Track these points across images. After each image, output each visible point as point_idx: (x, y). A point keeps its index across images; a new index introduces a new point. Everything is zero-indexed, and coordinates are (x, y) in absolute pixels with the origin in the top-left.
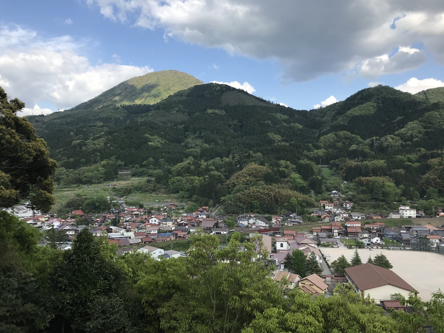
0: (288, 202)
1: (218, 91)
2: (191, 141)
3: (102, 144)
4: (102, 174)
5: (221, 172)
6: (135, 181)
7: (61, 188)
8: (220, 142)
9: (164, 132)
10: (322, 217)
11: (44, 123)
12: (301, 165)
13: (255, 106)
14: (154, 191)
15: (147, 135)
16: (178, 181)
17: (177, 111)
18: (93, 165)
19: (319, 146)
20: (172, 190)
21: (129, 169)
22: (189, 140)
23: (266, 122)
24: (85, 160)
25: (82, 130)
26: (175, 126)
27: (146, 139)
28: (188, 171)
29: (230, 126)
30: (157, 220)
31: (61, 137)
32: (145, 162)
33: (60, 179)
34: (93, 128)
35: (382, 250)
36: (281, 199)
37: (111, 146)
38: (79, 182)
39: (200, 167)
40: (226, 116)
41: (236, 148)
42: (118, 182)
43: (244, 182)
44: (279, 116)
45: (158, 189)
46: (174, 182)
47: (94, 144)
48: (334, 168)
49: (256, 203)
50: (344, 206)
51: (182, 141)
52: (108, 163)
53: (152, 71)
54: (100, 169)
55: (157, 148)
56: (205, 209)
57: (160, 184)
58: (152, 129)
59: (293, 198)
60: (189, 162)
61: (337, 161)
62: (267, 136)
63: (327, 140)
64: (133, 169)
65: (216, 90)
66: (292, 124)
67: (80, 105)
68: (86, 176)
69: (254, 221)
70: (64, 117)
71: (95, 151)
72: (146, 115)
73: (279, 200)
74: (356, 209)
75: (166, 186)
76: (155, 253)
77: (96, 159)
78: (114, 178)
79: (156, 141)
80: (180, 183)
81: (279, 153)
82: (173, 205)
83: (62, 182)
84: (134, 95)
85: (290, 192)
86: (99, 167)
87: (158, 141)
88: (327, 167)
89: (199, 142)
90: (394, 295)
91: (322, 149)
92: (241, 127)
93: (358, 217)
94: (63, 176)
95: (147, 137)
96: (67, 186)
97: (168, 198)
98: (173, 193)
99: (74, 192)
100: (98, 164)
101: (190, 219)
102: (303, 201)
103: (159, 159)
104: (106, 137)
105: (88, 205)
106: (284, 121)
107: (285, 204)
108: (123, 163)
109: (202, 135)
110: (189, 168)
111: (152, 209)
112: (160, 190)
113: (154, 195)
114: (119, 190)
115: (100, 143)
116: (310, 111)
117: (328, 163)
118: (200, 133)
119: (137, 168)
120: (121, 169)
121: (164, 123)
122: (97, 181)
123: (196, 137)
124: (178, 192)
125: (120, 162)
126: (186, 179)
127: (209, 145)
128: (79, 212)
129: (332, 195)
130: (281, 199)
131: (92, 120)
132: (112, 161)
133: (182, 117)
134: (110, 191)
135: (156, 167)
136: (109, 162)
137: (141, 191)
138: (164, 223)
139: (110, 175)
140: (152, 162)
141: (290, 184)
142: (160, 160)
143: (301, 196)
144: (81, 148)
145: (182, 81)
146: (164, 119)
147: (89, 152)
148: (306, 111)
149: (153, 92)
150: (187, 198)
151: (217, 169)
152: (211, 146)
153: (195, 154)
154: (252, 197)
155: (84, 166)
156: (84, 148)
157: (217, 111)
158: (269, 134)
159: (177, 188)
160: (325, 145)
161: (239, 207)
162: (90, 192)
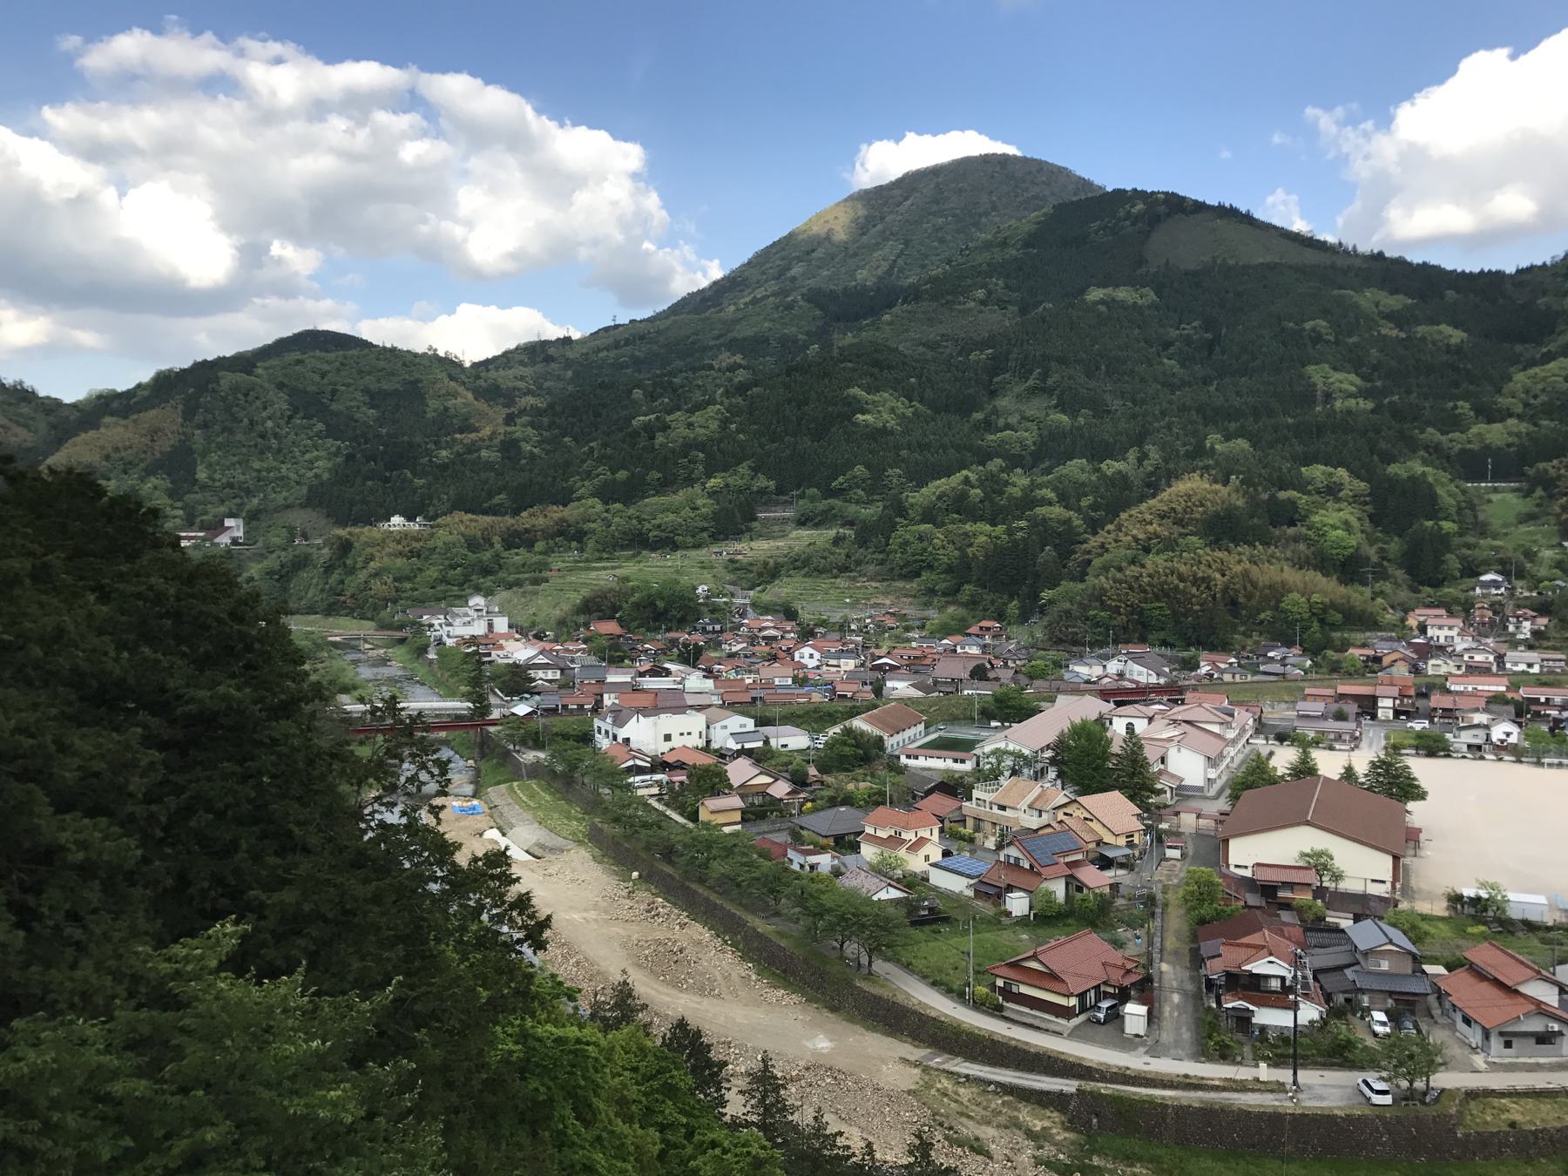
0: (1276, 608)
1: (1136, 219)
3: (714, 425)
4: (705, 518)
5: (1079, 510)
6: (801, 539)
7: (587, 561)
8: (1116, 404)
9: (919, 377)
10: (1386, 661)
11: (569, 364)
12: (1393, 482)
13: (1272, 267)
14: (844, 569)
15: (856, 391)
16: (921, 539)
18: (681, 493)
19: (1499, 411)
22: (1003, 403)
23: (1308, 325)
25: (670, 383)
26: (960, 354)
27: (850, 404)
28: (959, 505)
29: (1167, 345)
30: (817, 655)
31: (604, 406)
32: (841, 479)
35: (1517, 765)
36: (1249, 597)
37: (738, 431)
38: (640, 542)
39: (1001, 493)
40: (1157, 308)
41: (1169, 427)
42: (753, 544)
43: (1136, 540)
44: (1370, 299)
45: (858, 563)
46: (906, 543)
47: (690, 425)
48: (1539, 492)
49: (1158, 609)
50: (1511, 628)
51: (975, 406)
52: (727, 485)
53: (1019, 154)
54: (699, 502)
55: (884, 432)
56: (988, 629)
58: (876, 370)
59: (1295, 596)
61: (1550, 467)
62: (1301, 376)
63: (1540, 386)
64: (801, 502)
66: (1421, 330)
67: (684, 299)
69: (1120, 666)
70: (627, 342)
71: (689, 446)
72: (873, 323)
73: (1241, 600)
74: (1548, 639)
78: (742, 532)
79: (883, 410)
80: (925, 544)
81: (1323, 437)
82: (893, 614)
83: (591, 544)
85: (1291, 575)
87: (892, 410)
88: (1514, 490)
90: (1308, 855)
91: (1511, 422)
92: (1210, 347)
93: (1530, 665)
94: (593, 525)
95: (855, 397)
96: (605, 555)
97: (886, 593)
98: (903, 577)
99: (618, 572)
100: (697, 487)
101: (918, 653)
102: (1333, 605)
104: (726, 402)
105: (637, 606)
106: (1390, 317)
107: (1262, 616)
108: (772, 484)
109: (1050, 381)
110: (963, 496)
113: (842, 582)
114: (747, 568)
115: (706, 423)
116: (1520, 272)
117: (1519, 475)
118: (1044, 376)
119: (813, 499)
120: (766, 504)
121: (932, 346)
122: (689, 540)
123: (1027, 390)
124: (919, 575)
125: (762, 482)
127: (1074, 415)
128: (611, 627)
129: (1478, 591)
130: (1249, 597)
131: (711, 348)
132: (740, 476)
133: (996, 320)
134: (720, 571)
136: (730, 480)
138: (832, 662)
139: (731, 522)
140: (864, 481)
141: (1302, 547)
143: (1327, 588)
144: (652, 438)
145: (1027, 189)
146: (932, 334)
147: (673, 451)
148: (1499, 275)
150: (945, 594)
151: (1063, 499)
152: (1081, 420)
153: (1017, 449)
154: (1145, 591)
155: (657, 493)
156: (660, 439)
157: (1123, 294)
158: (1311, 369)
159: (916, 561)
160: (1526, 405)
161: (1097, 625)
162: (652, 570)
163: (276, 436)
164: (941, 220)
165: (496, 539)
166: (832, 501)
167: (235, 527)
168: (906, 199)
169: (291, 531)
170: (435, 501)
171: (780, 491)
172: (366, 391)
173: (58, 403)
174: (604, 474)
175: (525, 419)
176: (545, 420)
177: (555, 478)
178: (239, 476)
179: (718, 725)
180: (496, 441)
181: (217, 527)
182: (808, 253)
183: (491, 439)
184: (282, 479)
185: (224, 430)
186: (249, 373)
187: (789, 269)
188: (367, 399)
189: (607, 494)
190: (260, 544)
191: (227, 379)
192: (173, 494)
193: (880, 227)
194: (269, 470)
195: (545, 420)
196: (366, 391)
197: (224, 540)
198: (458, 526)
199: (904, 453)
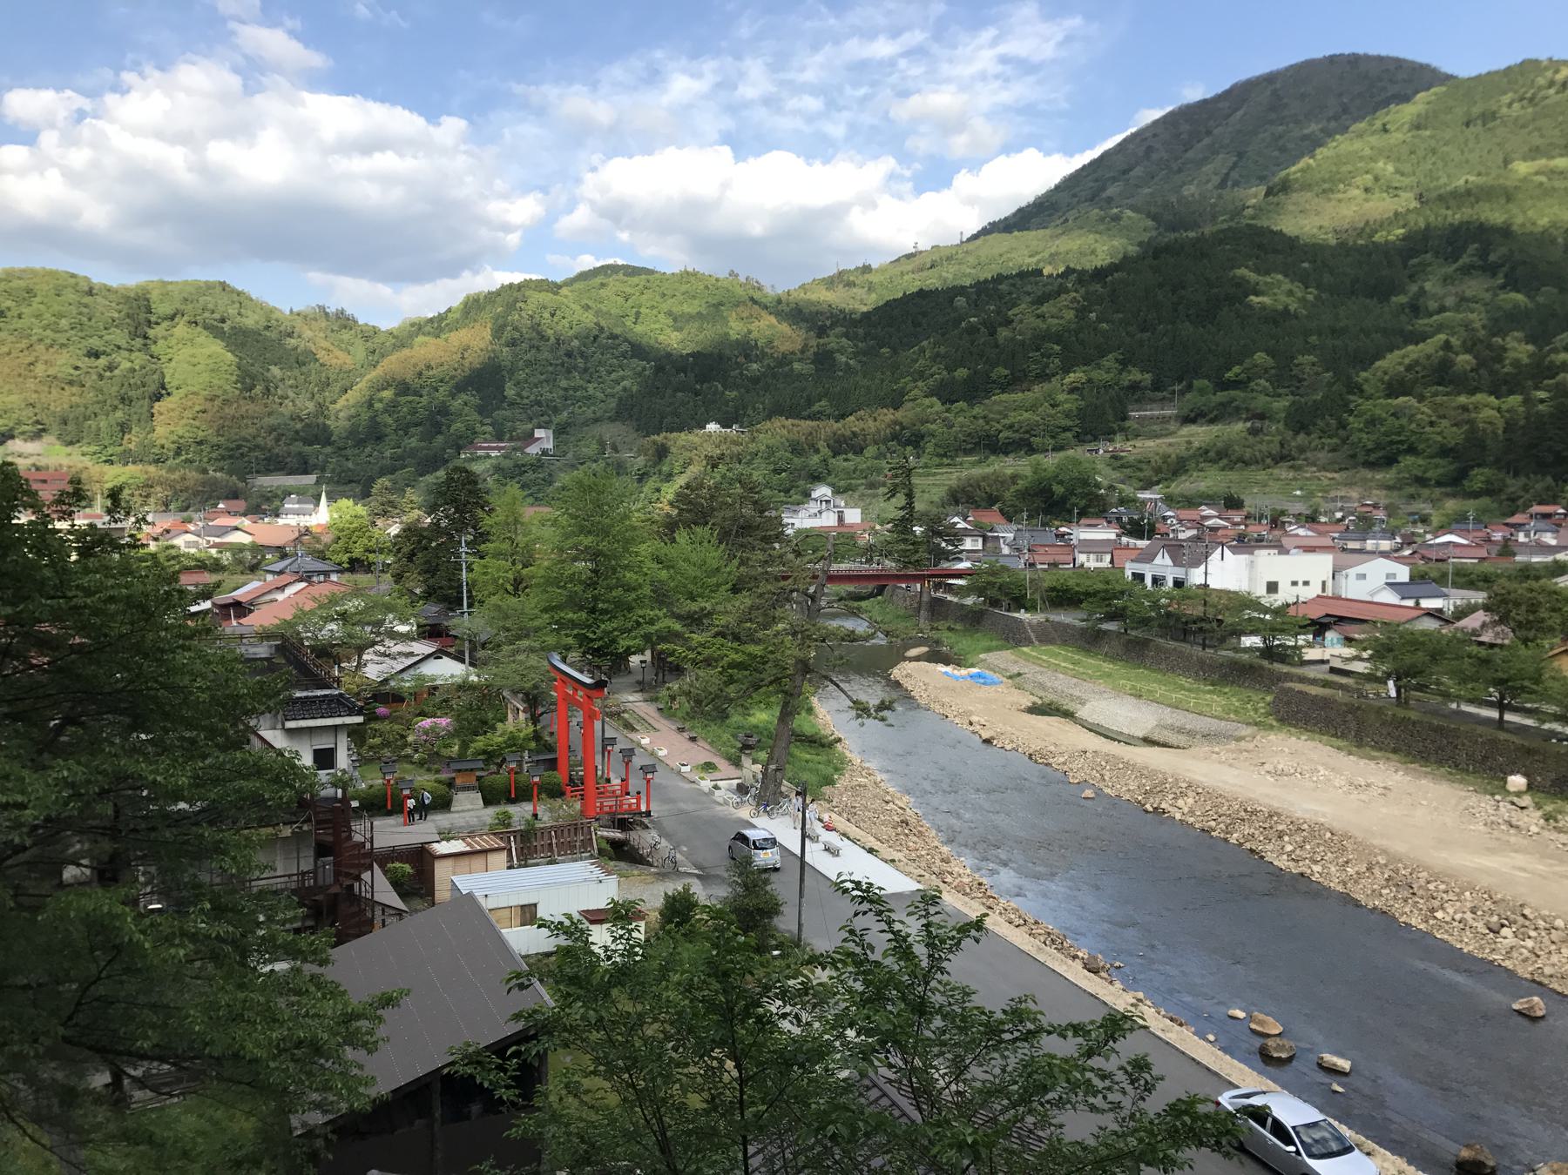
2: (1439, 290)
3: (1070, 315)
4: (1067, 415)
6: (1201, 434)
7: (926, 466)
17: (1367, 190)
20: (1369, 451)
21: (1171, 400)
24: (1007, 372)
31: (924, 314)
32: (1237, 369)
33: (922, 437)
34: (1032, 279)
37: (1100, 320)
45: (1302, 450)
47: (1041, 316)
54: (1061, 397)
57: (1308, 434)
60: (1447, 342)
64: (1188, 396)
65: (1551, 84)
68: (1011, 426)
71: (1040, 339)
75: (1335, 440)
76: (1362, 577)
77: (1047, 366)
80: (1404, 421)
83: (930, 448)
84: (1180, 171)
86: (1059, 394)
87: (1290, 293)
89: (1475, 287)
94: (933, 427)
95: (1242, 277)
96: (946, 461)
97: (1349, 484)
103: (1293, 358)
105: (1024, 495)
109: (1492, 258)
111: (1283, 513)
112: (1309, 454)
113: (1283, 472)
114: (1138, 465)
119: (1202, 392)
120: (1138, 401)
124: (1390, 461)
125: (1135, 375)
126: (1436, 407)
132: (1105, 371)
135: (1281, 391)
136: (1095, 375)
137: (1225, 461)
139: (1096, 423)
142: (1300, 359)
144: (993, 333)
147: (1023, 343)
149: (1119, 463)
150: (1439, 484)
152: (1540, 299)
156: (1003, 333)
159: (1392, 443)
163: (582, 354)
164: (1281, 128)
165: (821, 445)
166: (1233, 393)
167: (545, 438)
168: (1236, 110)
169: (602, 444)
170: (750, 412)
171: (1157, 386)
172: (669, 314)
173: (376, 331)
174: (939, 373)
175: (839, 330)
176: (861, 331)
177: (882, 381)
178: (546, 394)
179: (1353, 572)
180: (810, 353)
181: (530, 438)
182: (1125, 172)
183: (802, 352)
184: (589, 398)
185: (532, 347)
186: (556, 294)
187: (1103, 189)
188: (670, 321)
189: (947, 394)
190: (570, 455)
191: (536, 298)
192: (481, 410)
193: (1207, 141)
194: (576, 389)
195: (861, 331)
196: (669, 314)
197: (533, 450)
198: (778, 431)
199: (1313, 339)
